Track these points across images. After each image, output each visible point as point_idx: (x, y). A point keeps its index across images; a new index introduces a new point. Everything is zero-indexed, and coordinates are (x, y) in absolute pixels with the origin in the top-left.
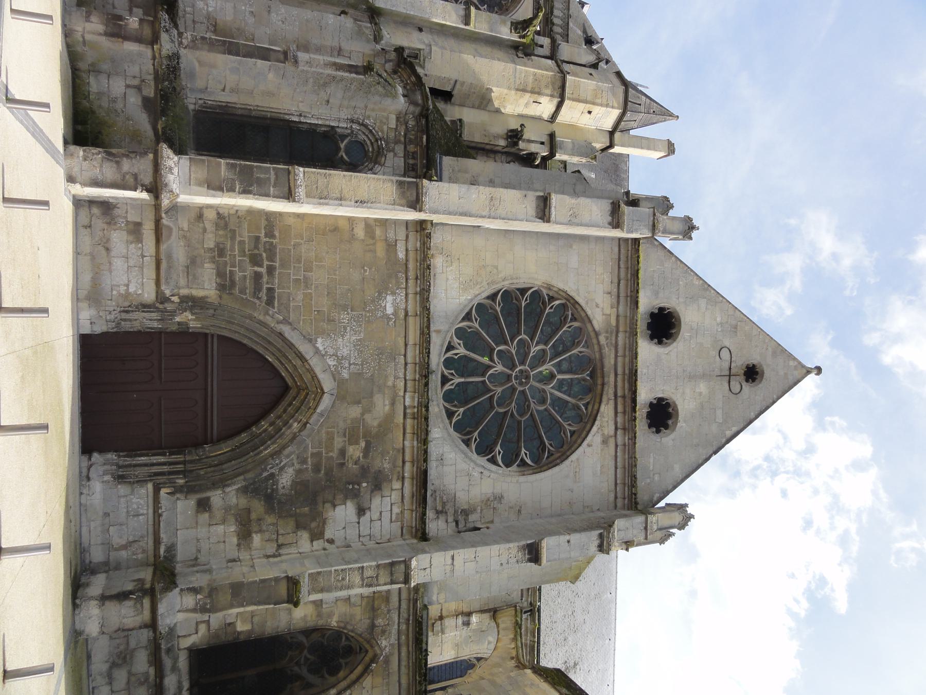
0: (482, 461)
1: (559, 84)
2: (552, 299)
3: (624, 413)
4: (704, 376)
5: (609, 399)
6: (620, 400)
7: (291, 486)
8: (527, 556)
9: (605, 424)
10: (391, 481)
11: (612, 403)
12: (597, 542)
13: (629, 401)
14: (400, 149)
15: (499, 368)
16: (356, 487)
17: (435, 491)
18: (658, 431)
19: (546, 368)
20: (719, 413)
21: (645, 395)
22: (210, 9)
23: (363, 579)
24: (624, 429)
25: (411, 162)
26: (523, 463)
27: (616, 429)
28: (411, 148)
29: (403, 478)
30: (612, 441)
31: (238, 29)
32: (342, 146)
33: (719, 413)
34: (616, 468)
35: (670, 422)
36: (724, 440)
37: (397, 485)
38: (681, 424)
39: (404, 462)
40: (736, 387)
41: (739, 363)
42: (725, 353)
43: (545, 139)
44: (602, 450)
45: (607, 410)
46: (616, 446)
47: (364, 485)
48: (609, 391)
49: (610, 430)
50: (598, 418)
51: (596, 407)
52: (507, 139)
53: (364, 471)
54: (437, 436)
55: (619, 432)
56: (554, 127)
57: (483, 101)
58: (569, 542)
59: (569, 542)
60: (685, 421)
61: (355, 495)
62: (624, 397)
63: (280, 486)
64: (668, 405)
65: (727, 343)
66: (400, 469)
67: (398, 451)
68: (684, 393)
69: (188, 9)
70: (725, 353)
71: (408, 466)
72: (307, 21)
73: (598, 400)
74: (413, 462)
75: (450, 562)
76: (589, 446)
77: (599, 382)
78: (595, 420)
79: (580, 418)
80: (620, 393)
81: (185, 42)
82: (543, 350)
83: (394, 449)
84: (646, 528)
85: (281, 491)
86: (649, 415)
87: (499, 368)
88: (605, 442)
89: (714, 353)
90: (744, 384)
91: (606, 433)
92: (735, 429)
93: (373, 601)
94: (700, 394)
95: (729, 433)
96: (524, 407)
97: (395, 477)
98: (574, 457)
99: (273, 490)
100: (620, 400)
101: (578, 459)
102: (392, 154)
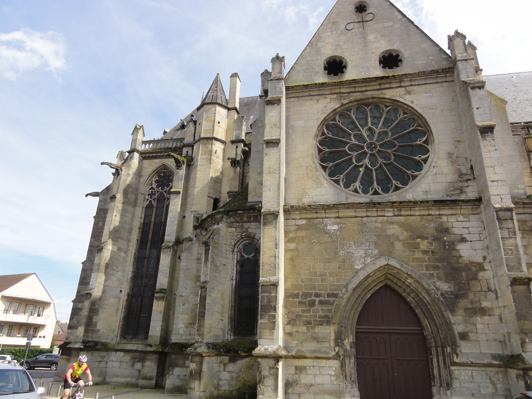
0: (426, 167)
1: (205, 141)
2: (323, 134)
3: (390, 83)
4: (364, 38)
5: (382, 93)
6: (382, 87)
7: (448, 283)
8: (489, 134)
9: (398, 94)
10: (442, 222)
11: (384, 91)
12: (477, 90)
13: (383, 81)
14: (246, 225)
15: (366, 161)
16: (447, 243)
17: (447, 195)
18: (401, 61)
19: (365, 133)
20: (387, 24)
21: (378, 72)
22: (183, 326)
23: (511, 238)
24: (400, 82)
25: (252, 219)
26: (426, 142)
27: (400, 87)
28: (245, 219)
29: (439, 215)
30: (408, 88)
31: (192, 312)
32: (246, 257)
33: (387, 24)
34: (426, 84)
35: (394, 54)
36: (404, 19)
37: (444, 219)
38: (395, 47)
39: (429, 215)
40: (370, 17)
41: (355, 17)
42: (349, 27)
43: (234, 146)
44: (415, 94)
45: (389, 94)
46: (412, 85)
47: (445, 238)
48: (377, 94)
49: (401, 91)
50: (394, 98)
51: (387, 101)
52: (236, 167)
53: (436, 239)
54: (411, 196)
55: (402, 84)
56: (228, 142)
57: (217, 181)
58: (478, 108)
59: (478, 108)
60: (393, 45)
61: (452, 244)
62: (380, 84)
63: (449, 290)
64: (384, 57)
65: (343, 27)
66: (434, 217)
67: (422, 218)
68: (375, 48)
69: (184, 338)
70: (349, 27)
71: (431, 212)
72: (185, 276)
73: (383, 100)
74: (429, 210)
75: (495, 183)
76: (412, 102)
77: (371, 100)
78: (396, 100)
79: (396, 110)
80: (378, 87)
81: (200, 340)
82: (355, 136)
83: (421, 221)
84: (466, 60)
85: (452, 289)
86: (391, 67)
87: (366, 161)
88: (409, 93)
89: (350, 33)
90: (367, 12)
91: (404, 93)
92: (397, 13)
93: (526, 230)
94: (375, 38)
95: (400, 16)
96: (391, 144)
97: (439, 220)
98: (420, 111)
99: (451, 294)
100: (382, 87)
101: (422, 108)
102: (249, 229)
